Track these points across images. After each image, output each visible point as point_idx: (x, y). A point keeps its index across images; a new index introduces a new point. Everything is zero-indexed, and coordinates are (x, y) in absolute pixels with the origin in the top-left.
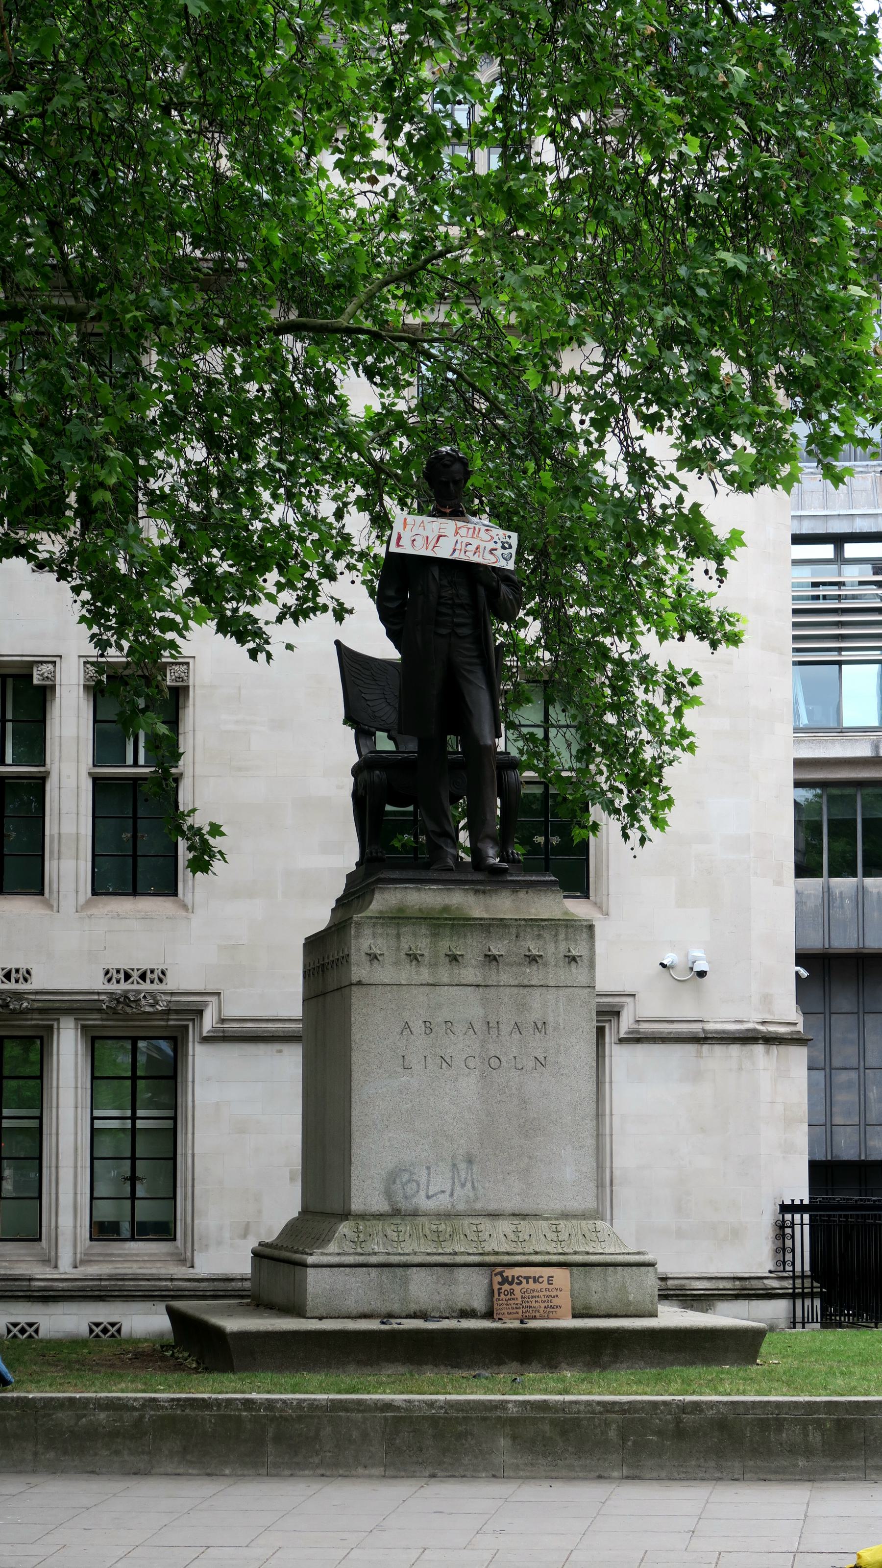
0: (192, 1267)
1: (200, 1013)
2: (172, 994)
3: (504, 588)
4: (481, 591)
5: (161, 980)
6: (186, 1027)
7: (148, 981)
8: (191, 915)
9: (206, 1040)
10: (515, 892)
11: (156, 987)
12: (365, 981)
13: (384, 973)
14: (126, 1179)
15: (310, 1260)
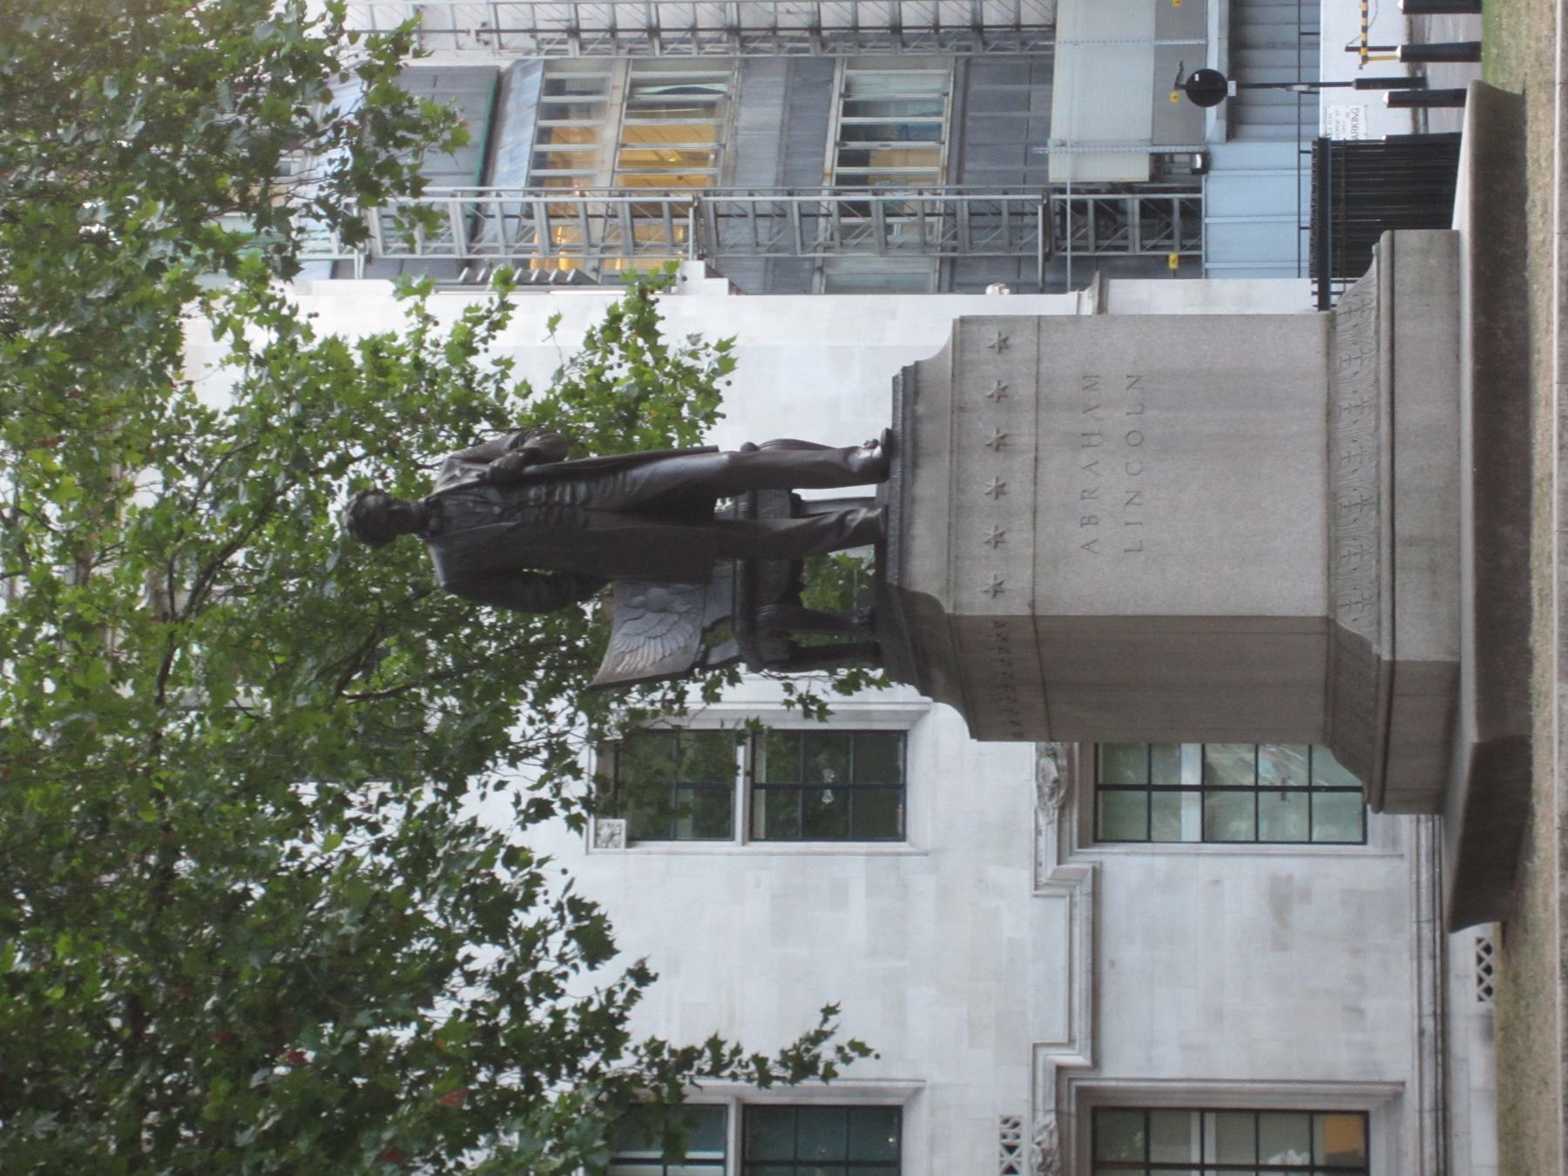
0: (1403, 1084)
1: (1060, 1069)
2: (1034, 1110)
3: (528, 444)
4: (531, 469)
5: (1016, 1125)
6: (1080, 1090)
7: (1016, 1142)
8: (929, 1083)
9: (1096, 1063)
10: (913, 501)
11: (1025, 1130)
12: (1029, 598)
13: (1019, 581)
14: (1283, 798)
15: (1386, 657)
